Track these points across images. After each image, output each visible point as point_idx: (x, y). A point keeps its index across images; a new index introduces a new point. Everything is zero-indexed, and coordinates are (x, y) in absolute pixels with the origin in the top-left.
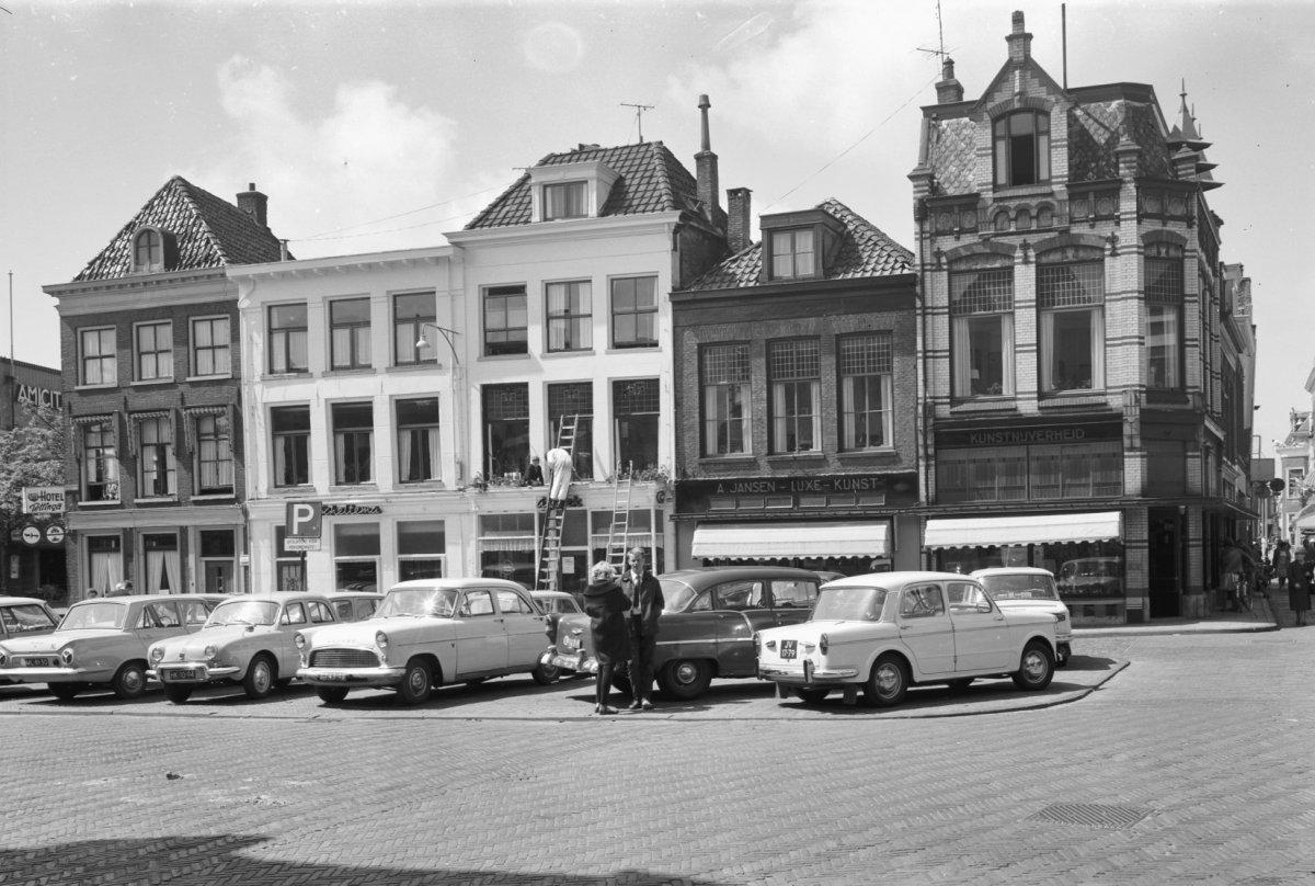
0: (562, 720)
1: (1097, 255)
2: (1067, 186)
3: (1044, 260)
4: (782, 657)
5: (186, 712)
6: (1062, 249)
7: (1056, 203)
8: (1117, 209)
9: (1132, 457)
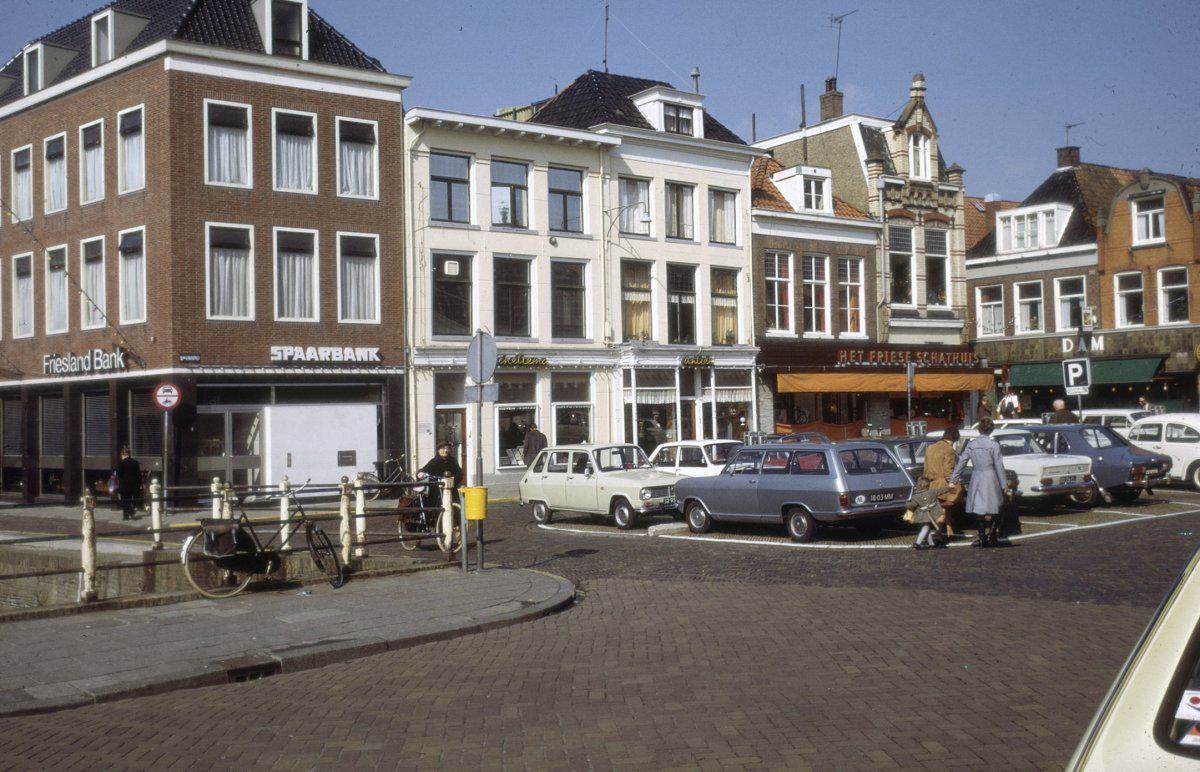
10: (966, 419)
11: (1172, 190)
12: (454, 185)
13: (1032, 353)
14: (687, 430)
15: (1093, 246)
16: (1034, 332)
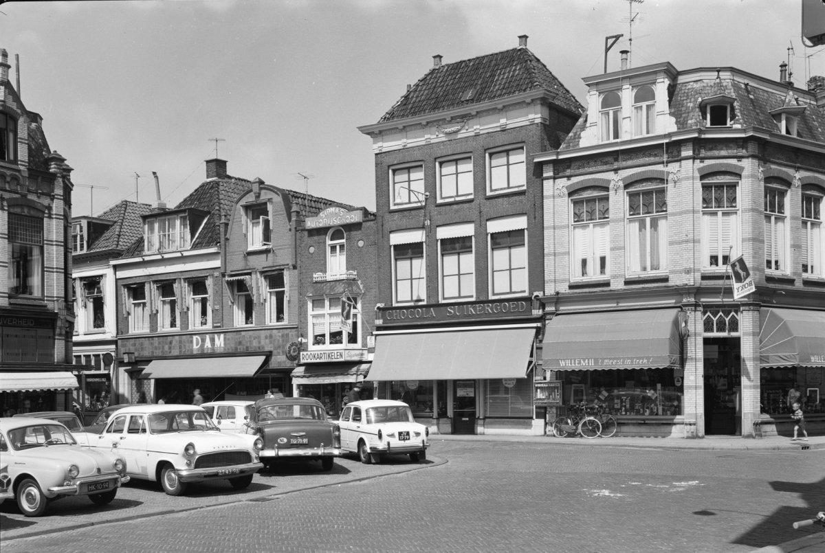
0: (286, 493)
1: (40, 215)
2: (28, 169)
3: (12, 210)
4: (400, 440)
5: (100, 520)
6: (21, 206)
7: (21, 177)
8: (53, 191)
9: (60, 339)
10: (784, 545)
11: (278, 199)
12: (495, 270)
13: (170, 348)
14: (228, 484)
15: (213, 250)
16: (173, 329)
